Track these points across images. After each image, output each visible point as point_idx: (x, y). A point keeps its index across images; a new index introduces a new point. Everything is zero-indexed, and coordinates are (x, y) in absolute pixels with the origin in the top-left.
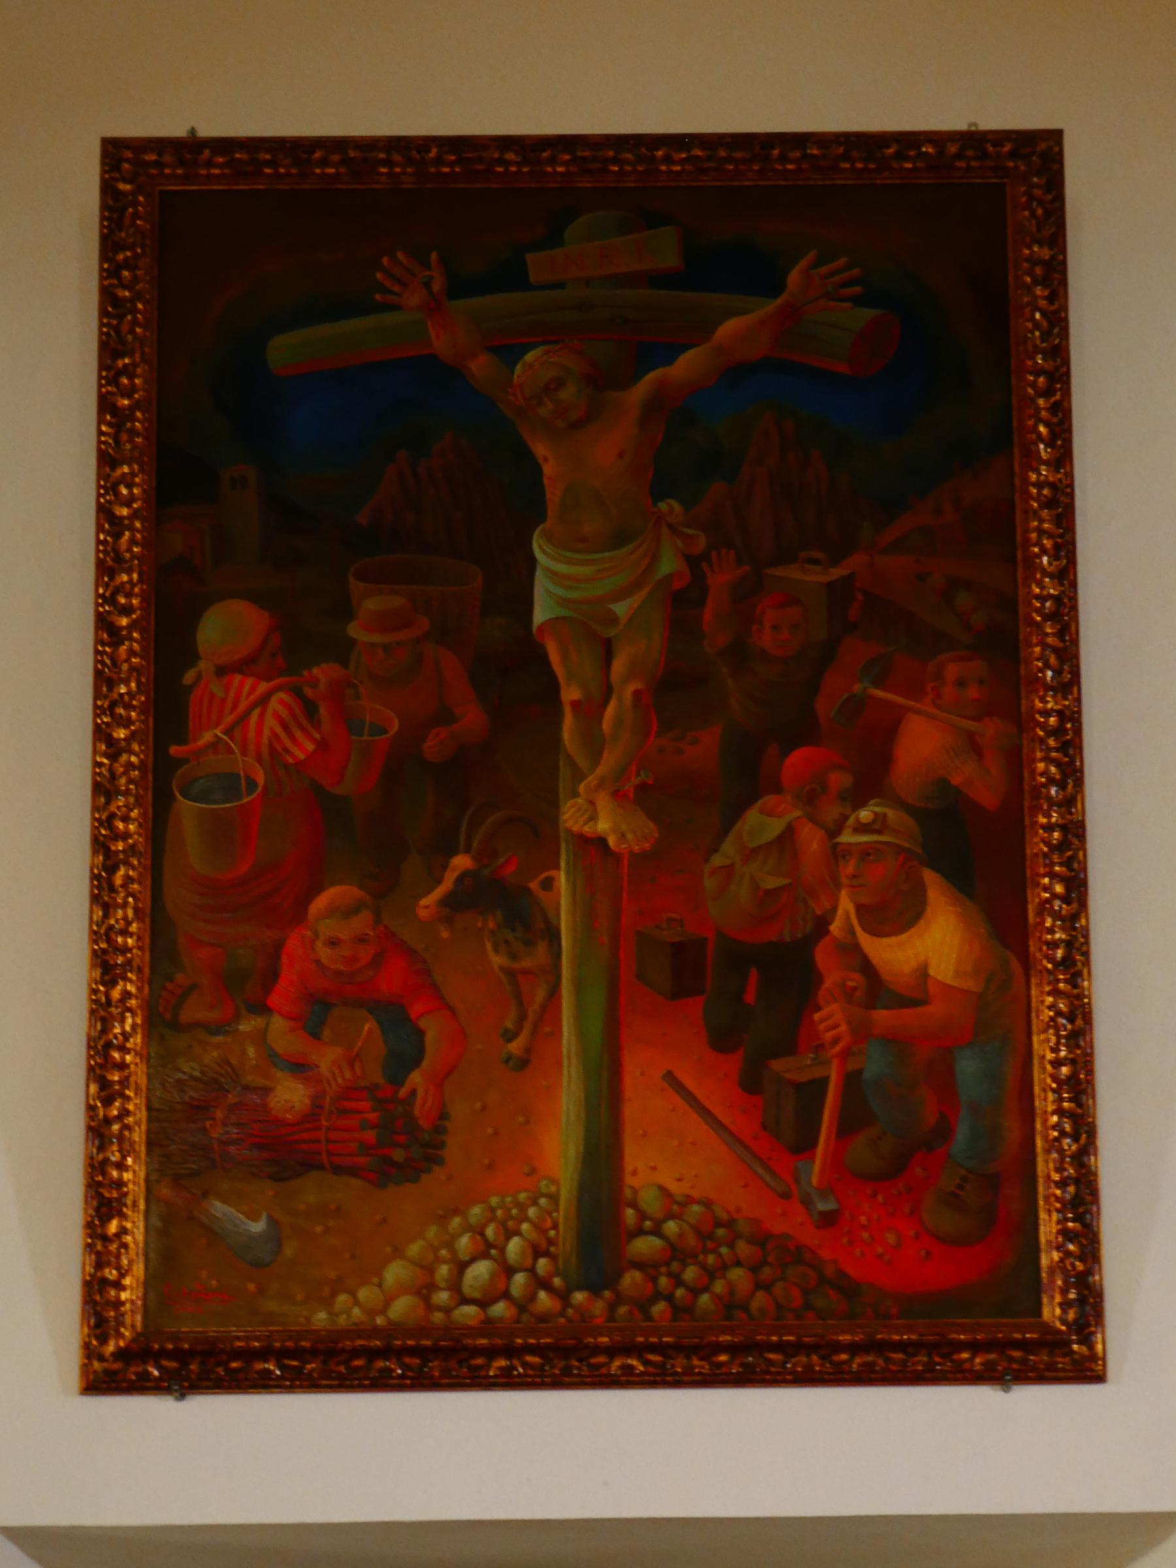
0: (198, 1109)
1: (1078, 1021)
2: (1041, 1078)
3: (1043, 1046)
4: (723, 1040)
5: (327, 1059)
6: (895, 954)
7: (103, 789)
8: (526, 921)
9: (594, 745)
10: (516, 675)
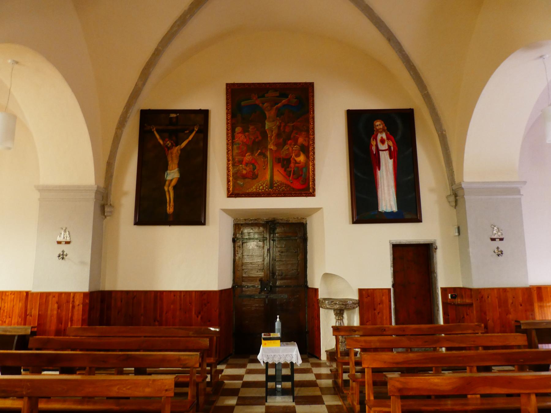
0: (236, 173)
1: (314, 165)
2: (310, 170)
3: (311, 167)
4: (282, 167)
5: (248, 169)
6: (298, 159)
7: (227, 144)
8: (265, 156)
9: (271, 140)
10: (264, 134)
